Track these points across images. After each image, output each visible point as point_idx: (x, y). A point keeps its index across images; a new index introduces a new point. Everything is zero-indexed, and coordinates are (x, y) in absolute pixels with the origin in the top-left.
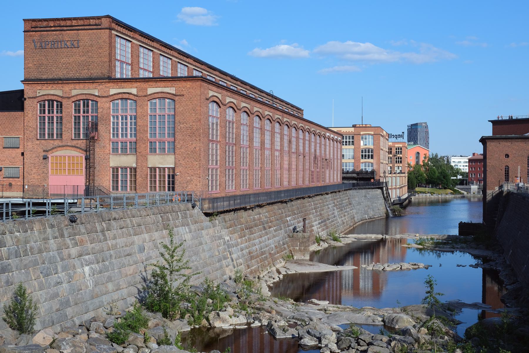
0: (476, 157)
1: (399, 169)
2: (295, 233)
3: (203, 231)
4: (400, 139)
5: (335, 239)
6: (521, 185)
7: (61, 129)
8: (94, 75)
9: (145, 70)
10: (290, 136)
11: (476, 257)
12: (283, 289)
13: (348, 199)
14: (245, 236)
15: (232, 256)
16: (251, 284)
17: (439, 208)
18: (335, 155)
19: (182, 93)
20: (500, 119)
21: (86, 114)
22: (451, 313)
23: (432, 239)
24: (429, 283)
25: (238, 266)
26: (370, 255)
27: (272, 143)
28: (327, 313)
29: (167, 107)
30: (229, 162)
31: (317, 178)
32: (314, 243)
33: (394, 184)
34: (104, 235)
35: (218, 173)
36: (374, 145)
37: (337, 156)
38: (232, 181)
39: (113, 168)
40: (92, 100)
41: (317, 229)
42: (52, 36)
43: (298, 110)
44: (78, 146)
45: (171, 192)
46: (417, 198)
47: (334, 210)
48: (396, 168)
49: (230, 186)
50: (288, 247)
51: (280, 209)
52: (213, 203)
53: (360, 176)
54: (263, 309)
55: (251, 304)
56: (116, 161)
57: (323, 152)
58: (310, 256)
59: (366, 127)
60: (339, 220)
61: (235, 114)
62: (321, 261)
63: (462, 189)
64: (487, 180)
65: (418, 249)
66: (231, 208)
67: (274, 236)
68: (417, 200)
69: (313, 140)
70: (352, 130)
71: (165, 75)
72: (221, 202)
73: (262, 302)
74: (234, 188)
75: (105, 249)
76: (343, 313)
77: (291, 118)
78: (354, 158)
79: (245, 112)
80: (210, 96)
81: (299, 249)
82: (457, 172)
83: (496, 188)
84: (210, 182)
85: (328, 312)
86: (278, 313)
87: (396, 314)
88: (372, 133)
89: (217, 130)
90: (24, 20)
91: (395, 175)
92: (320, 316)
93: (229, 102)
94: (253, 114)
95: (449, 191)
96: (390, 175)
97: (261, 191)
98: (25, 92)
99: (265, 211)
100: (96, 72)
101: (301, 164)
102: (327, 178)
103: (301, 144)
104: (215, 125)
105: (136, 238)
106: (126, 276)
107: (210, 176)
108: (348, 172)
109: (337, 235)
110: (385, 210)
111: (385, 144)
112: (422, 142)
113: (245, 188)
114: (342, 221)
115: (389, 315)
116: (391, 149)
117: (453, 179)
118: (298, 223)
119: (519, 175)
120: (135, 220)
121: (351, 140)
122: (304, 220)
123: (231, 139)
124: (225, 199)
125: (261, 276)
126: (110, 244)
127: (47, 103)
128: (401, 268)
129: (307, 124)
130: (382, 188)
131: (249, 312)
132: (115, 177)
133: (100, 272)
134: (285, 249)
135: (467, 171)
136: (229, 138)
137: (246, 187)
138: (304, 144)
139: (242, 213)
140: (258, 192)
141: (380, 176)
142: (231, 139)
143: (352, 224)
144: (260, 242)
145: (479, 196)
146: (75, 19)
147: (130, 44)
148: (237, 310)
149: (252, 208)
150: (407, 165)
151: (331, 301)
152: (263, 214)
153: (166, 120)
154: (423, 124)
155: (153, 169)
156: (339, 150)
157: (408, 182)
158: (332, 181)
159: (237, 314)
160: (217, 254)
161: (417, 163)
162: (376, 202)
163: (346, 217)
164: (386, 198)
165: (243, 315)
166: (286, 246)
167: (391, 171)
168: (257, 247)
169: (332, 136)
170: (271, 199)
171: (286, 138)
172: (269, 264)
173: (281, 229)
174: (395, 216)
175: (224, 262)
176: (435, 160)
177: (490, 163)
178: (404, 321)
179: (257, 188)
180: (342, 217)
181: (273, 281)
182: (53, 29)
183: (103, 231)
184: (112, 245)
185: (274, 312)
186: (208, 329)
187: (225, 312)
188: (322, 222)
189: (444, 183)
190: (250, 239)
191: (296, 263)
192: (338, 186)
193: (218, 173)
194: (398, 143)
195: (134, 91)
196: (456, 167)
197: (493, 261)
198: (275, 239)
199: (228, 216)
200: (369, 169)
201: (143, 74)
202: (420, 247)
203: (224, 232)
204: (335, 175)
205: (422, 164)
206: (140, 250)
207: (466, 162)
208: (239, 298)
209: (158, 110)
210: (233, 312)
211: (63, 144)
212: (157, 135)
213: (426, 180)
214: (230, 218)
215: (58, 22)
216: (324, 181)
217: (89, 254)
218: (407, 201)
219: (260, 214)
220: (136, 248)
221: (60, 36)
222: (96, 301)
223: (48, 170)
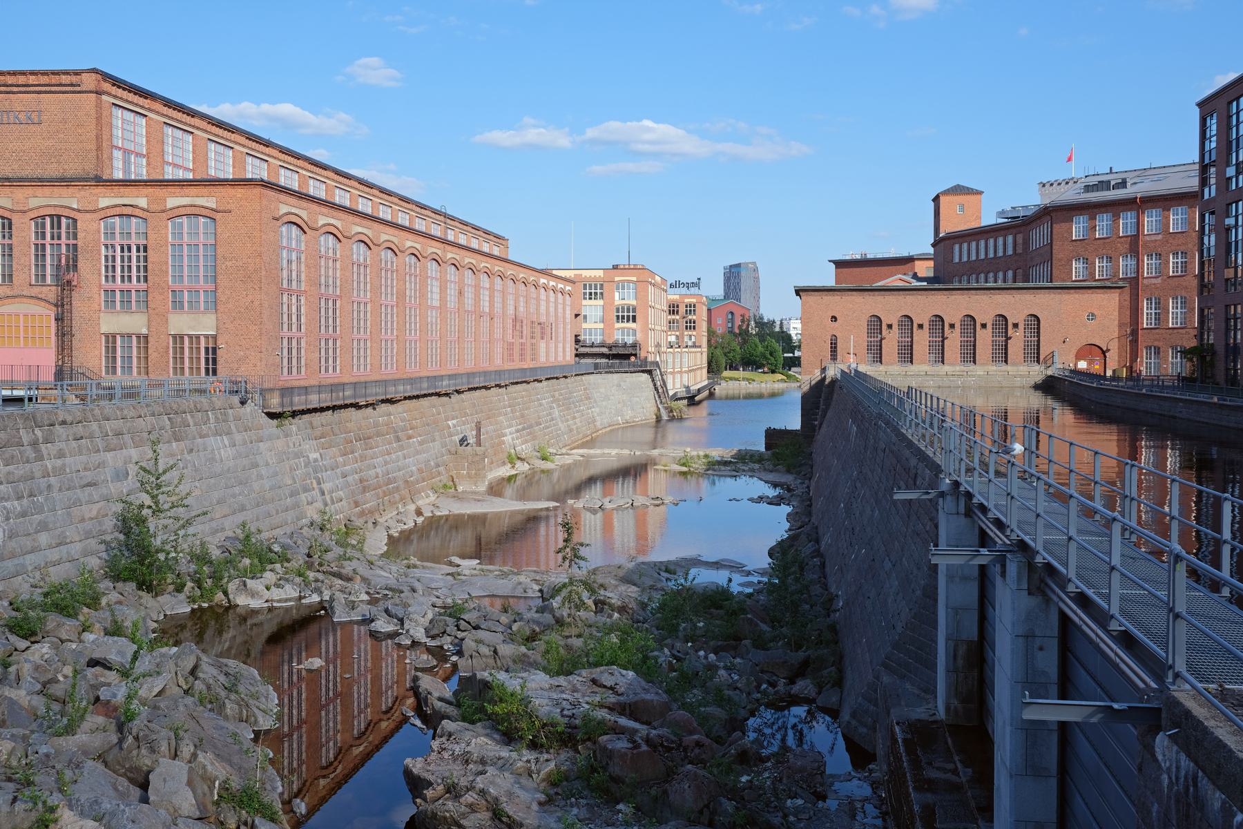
7: (11, 266)
8: (69, 174)
9: (175, 165)
14: (352, 452)
19: (228, 207)
21: (56, 242)
23: (706, 456)
29: (201, 230)
32: (504, 464)
33: (678, 365)
34: (37, 451)
35: (303, 344)
39: (107, 336)
40: (68, 218)
44: (42, 296)
45: (211, 378)
47: (552, 408)
48: (686, 339)
50: (448, 471)
53: (614, 352)
56: (111, 323)
65: (675, 474)
67: (418, 453)
71: (221, 176)
75: (38, 474)
80: (281, 213)
84: (285, 361)
88: (634, 279)
93: (324, 225)
95: (780, 377)
100: (72, 169)
105: (109, 455)
106: (83, 520)
120: (109, 426)
127: (48, 220)
130: (650, 372)
133: (24, 514)
134: (439, 474)
141: (649, 352)
144: (386, 463)
146: (33, 73)
147: (144, 120)
155: (179, 338)
163: (578, 420)
164: (660, 390)
166: (441, 469)
168: (379, 470)
173: (434, 440)
174: (672, 419)
175: (303, 496)
181: (402, 527)
183: (34, 444)
184: (53, 468)
186: (227, 609)
188: (524, 429)
190: (363, 458)
195: (143, 202)
200: (630, 340)
201: (170, 173)
206: (118, 475)
209: (185, 235)
219: (390, 414)
220: (108, 473)
221: (7, 103)
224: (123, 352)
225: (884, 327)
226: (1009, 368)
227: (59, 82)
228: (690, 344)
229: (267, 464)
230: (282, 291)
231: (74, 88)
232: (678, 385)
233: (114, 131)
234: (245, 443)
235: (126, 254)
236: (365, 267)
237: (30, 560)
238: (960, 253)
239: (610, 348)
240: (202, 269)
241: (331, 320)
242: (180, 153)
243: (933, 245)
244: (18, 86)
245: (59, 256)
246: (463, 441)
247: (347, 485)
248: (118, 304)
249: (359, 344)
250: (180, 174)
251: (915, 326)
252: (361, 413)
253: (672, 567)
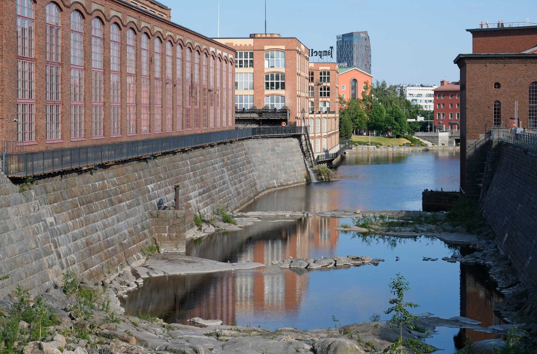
0: (446, 88)
1: (325, 105)
2: (161, 211)
3: (9, 208)
4: (326, 59)
5: (226, 220)
6: (519, 130)
10: (151, 52)
11: (451, 245)
12: (141, 303)
13: (246, 154)
14: (79, 216)
15: (59, 249)
16: (91, 295)
17: (390, 167)
18: (224, 82)
20: (485, 27)
22: (419, 334)
24: (398, 288)
25: (68, 266)
26: (280, 243)
27: (87, 56)
28: (221, 340)
30: (51, 94)
31: (196, 121)
32: (192, 226)
33: (318, 130)
35: (34, 111)
36: (285, 67)
37: (227, 85)
38: (57, 125)
41: (196, 203)
43: (161, 10)
46: (355, 153)
47: (223, 172)
48: (321, 105)
49: (54, 134)
50: (151, 232)
51: (136, 171)
52: (26, 161)
53: (264, 117)
54: (115, 336)
55: (93, 327)
57: (204, 78)
58: (187, 247)
59: (272, 38)
60: (232, 189)
61: (60, 14)
62: (203, 255)
63: (424, 138)
64: (467, 123)
65: (359, 234)
66: (56, 170)
67: (128, 216)
68: (354, 156)
69: (188, 58)
70: (251, 42)
72: (38, 160)
73: (113, 325)
74: (60, 137)
76: (246, 340)
77: (153, 22)
79: (78, 10)
81: (169, 235)
82: (416, 111)
83: (481, 135)
84: (20, 127)
85: (222, 338)
86: (140, 341)
87: (333, 339)
88: (283, 47)
89: (30, 41)
91: (319, 115)
92: (211, 345)
94: (91, 14)
95: (406, 141)
96: (312, 116)
97: (104, 142)
99: (111, 174)
101: (169, 97)
102: (212, 120)
103: (169, 65)
104: (27, 33)
107: (20, 117)
108: (243, 111)
109: (228, 213)
110: (305, 172)
111: (304, 67)
112: (360, 63)
113: (78, 136)
114: (237, 189)
115: (322, 340)
116: (312, 74)
117: (410, 123)
118: (166, 194)
119: (516, 116)
121: (249, 59)
122: (176, 188)
123: (54, 56)
124: (46, 156)
125: (108, 281)
128: (335, 265)
129: (179, 31)
130: (298, 137)
131: (93, 341)
134: (145, 236)
135: (432, 109)
136: (51, 54)
137: (80, 135)
138: (174, 64)
139: (75, 178)
140: (99, 143)
141: (296, 117)
142: (54, 56)
143: (252, 195)
144: (105, 226)
145: (451, 148)
148: (71, 339)
149: (90, 170)
150: (338, 100)
151: (225, 321)
152: (109, 179)
154: (362, 35)
156: (230, 75)
157: (340, 126)
158: (219, 125)
159: (72, 345)
160: (34, 246)
161: (354, 96)
162: (291, 158)
163: (243, 183)
164: (306, 152)
165: (82, 347)
166: (146, 231)
167: (312, 109)
168: (100, 233)
169: (219, 52)
170: (122, 154)
171: (145, 55)
172: (119, 262)
173: (138, 204)
174: (321, 182)
175: (45, 259)
176: (381, 91)
177: (471, 96)
178: (347, 349)
179: (98, 137)
180: (235, 184)
181: (126, 289)
185: (134, 341)
187: (52, 343)
188: (204, 192)
189: (396, 129)
190: (87, 222)
191: (164, 259)
192: (229, 132)
193: (34, 111)
194: (324, 64)
196: (415, 103)
197: (480, 250)
198: (128, 220)
199: (50, 184)
200: (279, 106)
202: (364, 230)
203: (45, 210)
204: (224, 116)
205: (361, 98)
207: (430, 95)
208: (73, 319)
210: (64, 343)
213: (368, 124)
214: (55, 186)
216: (207, 125)
218: (339, 157)
219: (103, 179)
229: (15, 229)
239: (260, 113)
253: (420, 326)
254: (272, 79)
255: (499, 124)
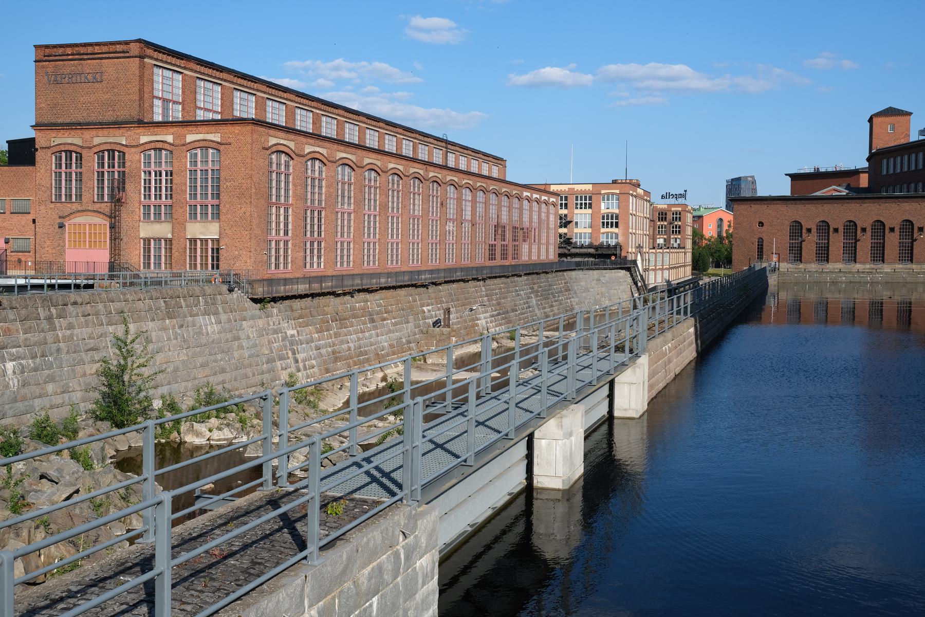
3: (244, 323)
7: (81, 188)
9: (206, 110)
14: (328, 330)
19: (229, 141)
21: (111, 170)
38: (319, 257)
39: (144, 240)
40: (119, 152)
42: (69, 67)
48: (672, 241)
53: (599, 252)
56: (147, 230)
67: (390, 331)
71: (245, 116)
78: (591, 227)
80: (270, 144)
88: (618, 191)
90: (35, 46)
98: (37, 141)
100: (123, 114)
120: (113, 307)
126: (60, 335)
130: (628, 269)
132: (147, 250)
133: (36, 369)
134: (410, 349)
144: (359, 339)
146: (98, 44)
152: (374, 301)
153: (210, 176)
155: (193, 241)
163: (555, 309)
164: (640, 285)
166: (413, 345)
173: (408, 322)
175: (278, 363)
182: (70, 57)
184: (64, 336)
188: (499, 314)
195: (170, 139)
200: (613, 242)
201: (200, 115)
209: (199, 163)
211: (84, 208)
212: (199, 196)
215: (77, 49)
217: (20, 346)
219: (367, 301)
221: (80, 68)
222: (20, 406)
223: (64, 242)
224: (155, 252)
225: (804, 231)
226: (914, 266)
227: (114, 50)
228: (676, 245)
229: (248, 338)
230: (270, 205)
231: (125, 54)
232: (659, 280)
233: (155, 86)
234: (229, 321)
235: (158, 178)
236: (350, 184)
237: (37, 403)
238: (888, 167)
239: (596, 248)
240: (210, 188)
241: (372, 230)
242: (210, 98)
243: (868, 160)
244: (87, 54)
245: (113, 180)
246: (436, 324)
247: (321, 355)
248: (152, 216)
249: (392, 246)
250: (210, 116)
251: (831, 230)
252: (338, 300)
254: (608, 219)
255: (762, 258)
